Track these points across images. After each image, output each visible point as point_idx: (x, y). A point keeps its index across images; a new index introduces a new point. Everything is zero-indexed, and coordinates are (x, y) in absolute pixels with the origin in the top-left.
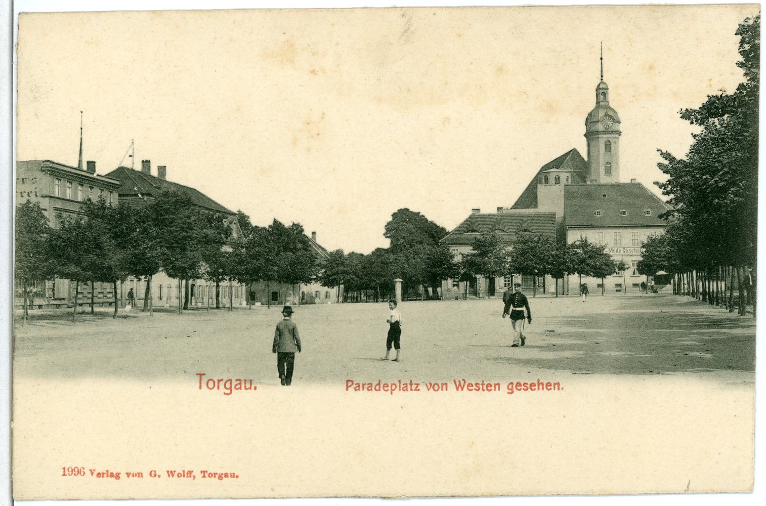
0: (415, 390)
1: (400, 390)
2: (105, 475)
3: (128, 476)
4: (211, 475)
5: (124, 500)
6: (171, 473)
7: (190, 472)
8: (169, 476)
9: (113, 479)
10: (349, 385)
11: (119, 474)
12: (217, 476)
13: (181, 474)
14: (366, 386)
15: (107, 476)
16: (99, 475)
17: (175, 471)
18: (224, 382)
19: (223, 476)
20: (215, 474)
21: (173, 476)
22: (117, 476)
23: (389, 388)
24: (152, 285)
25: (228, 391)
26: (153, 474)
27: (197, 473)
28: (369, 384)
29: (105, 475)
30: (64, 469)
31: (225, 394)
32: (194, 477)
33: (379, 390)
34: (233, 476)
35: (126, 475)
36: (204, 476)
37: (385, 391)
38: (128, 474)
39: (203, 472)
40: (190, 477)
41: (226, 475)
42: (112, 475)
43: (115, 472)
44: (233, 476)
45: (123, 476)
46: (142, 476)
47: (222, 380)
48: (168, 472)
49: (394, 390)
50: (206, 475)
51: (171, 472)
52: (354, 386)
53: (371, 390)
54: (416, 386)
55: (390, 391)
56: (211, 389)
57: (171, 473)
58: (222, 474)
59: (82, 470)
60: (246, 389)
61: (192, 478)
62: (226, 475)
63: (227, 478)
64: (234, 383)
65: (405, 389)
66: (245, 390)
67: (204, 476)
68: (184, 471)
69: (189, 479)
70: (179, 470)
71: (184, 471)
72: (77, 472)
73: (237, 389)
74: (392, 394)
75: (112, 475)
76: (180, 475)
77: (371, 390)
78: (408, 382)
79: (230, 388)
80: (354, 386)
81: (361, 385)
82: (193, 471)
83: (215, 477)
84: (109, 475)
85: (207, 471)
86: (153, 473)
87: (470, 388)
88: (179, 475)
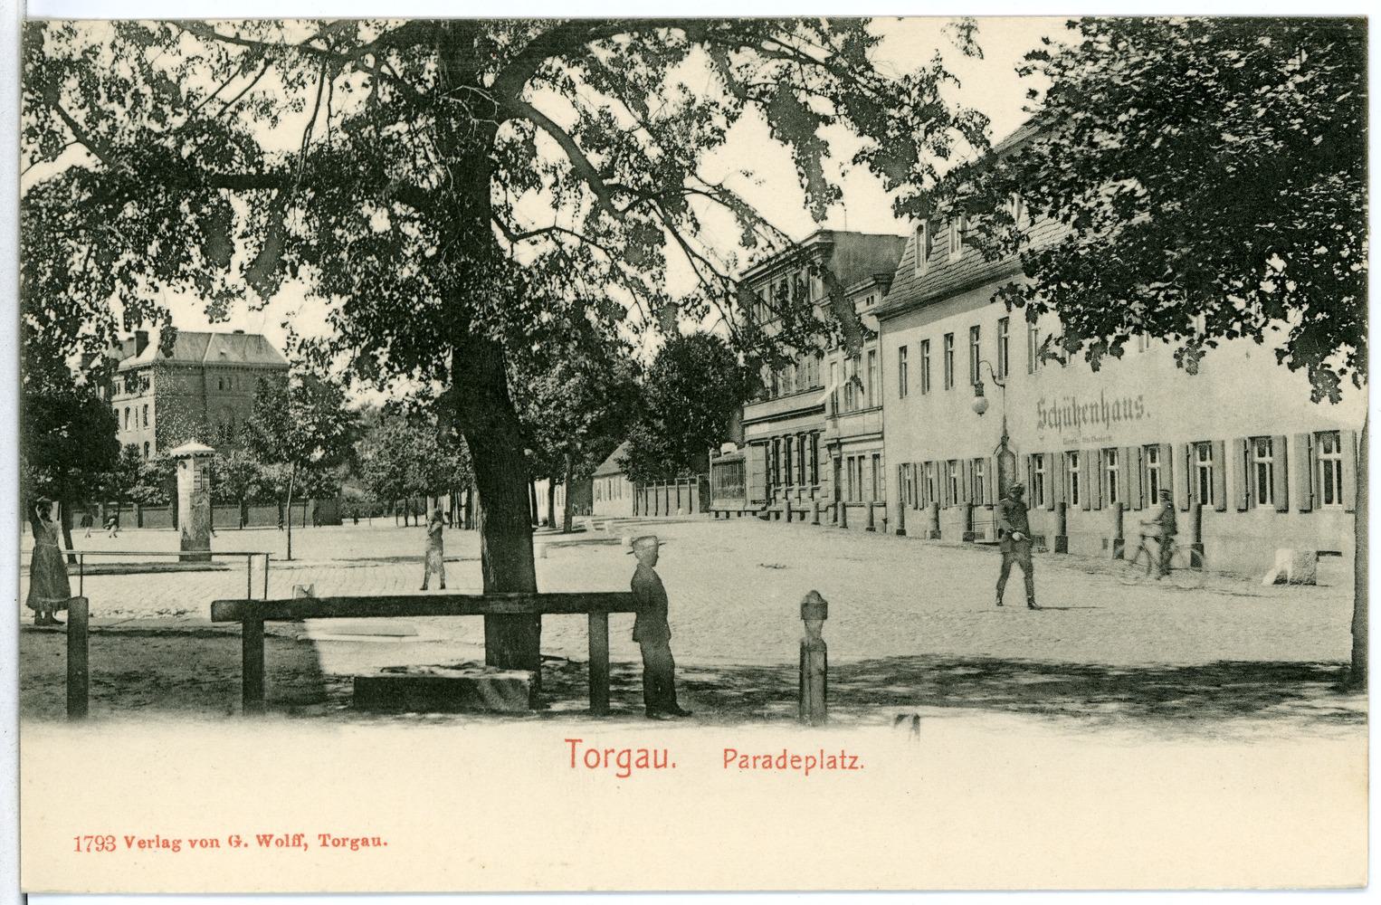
0: (851, 767)
1: (822, 767)
2: (154, 845)
3: (193, 845)
4: (336, 843)
6: (264, 840)
7: (299, 837)
8: (261, 844)
9: (169, 850)
10: (729, 758)
11: (179, 841)
12: (348, 843)
13: (282, 842)
14: (759, 762)
15: (158, 846)
16: (141, 844)
17: (271, 836)
19: (359, 843)
20: (344, 840)
21: (268, 845)
22: (176, 847)
23: (803, 763)
25: (625, 771)
26: (236, 841)
27: (311, 839)
28: (765, 757)
29: (154, 845)
30: (78, 838)
31: (618, 775)
32: (306, 845)
33: (784, 767)
34: (377, 842)
35: (189, 844)
36: (324, 844)
37: (795, 767)
38: (193, 844)
39: (324, 837)
40: (299, 845)
41: (365, 842)
42: (166, 844)
44: (377, 842)
45: (185, 845)
46: (217, 845)
48: (258, 836)
50: (329, 842)
51: (265, 836)
52: (738, 759)
53: (646, 765)
54: (855, 765)
55: (803, 770)
56: (592, 767)
57: (264, 840)
58: (357, 840)
59: (100, 847)
60: (843, 767)
61: (303, 847)
62: (365, 842)
63: (365, 848)
65: (832, 765)
66: (656, 770)
67: (324, 844)
68: (287, 836)
69: (297, 849)
70: (279, 835)
71: (287, 836)
72: (105, 844)
73: (641, 767)
74: (807, 774)
75: (166, 844)
77: (646, 765)
79: (628, 766)
81: (751, 761)
82: (303, 835)
83: (344, 845)
84: (161, 844)
85: (329, 836)
86: (234, 839)
87: (796, 764)
88: (279, 843)
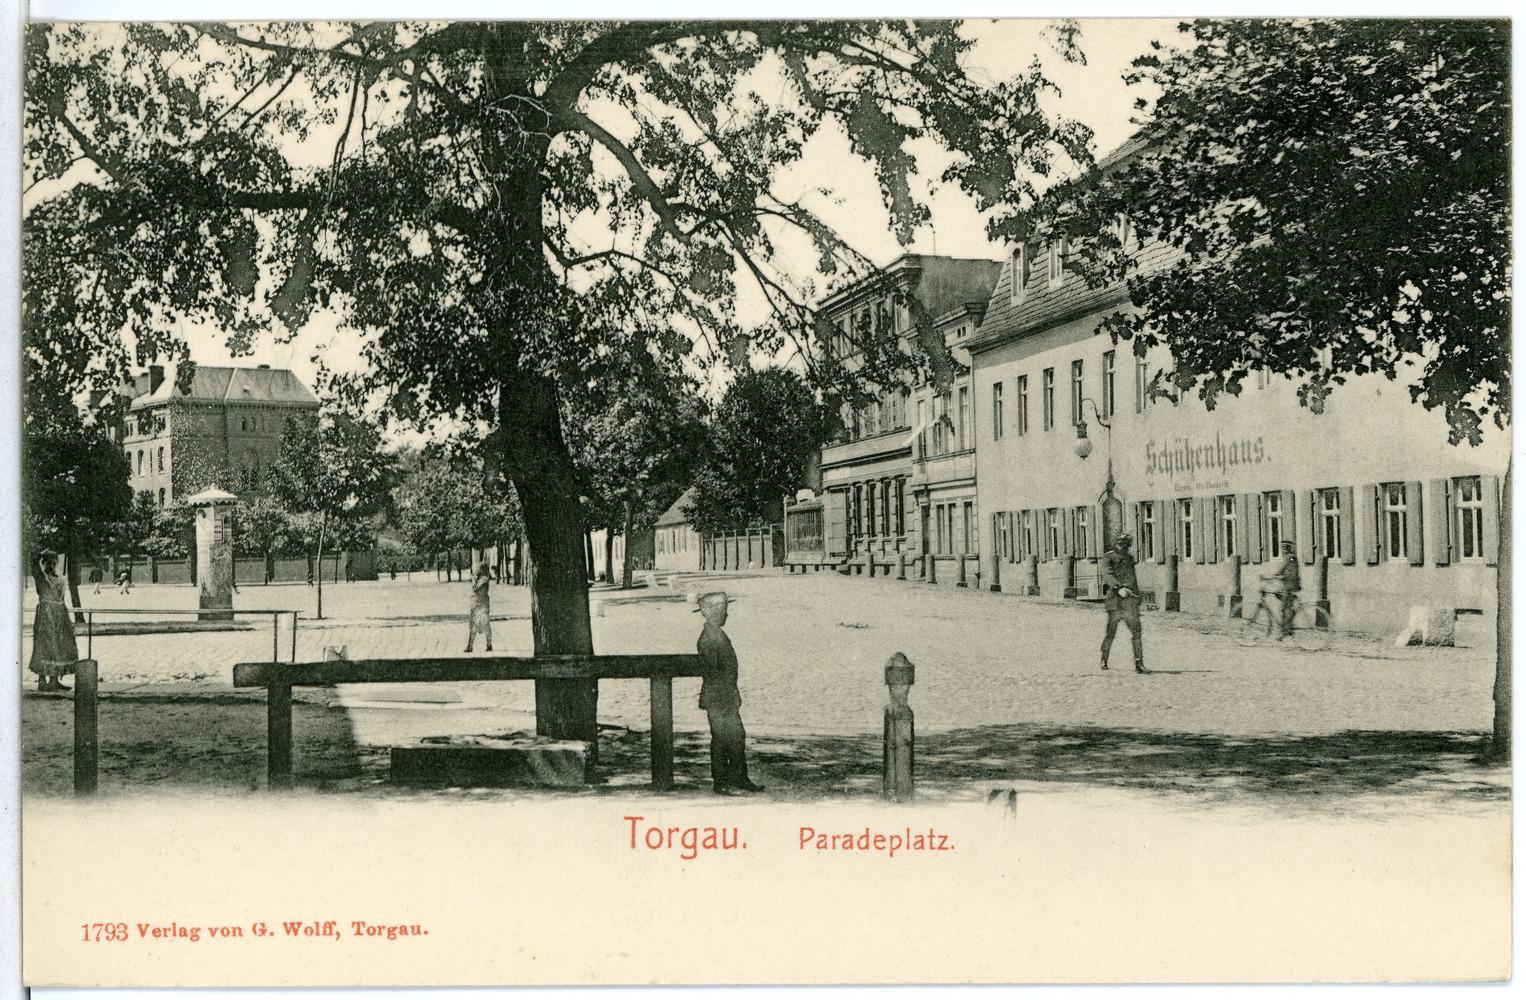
0: (940, 848)
1: (908, 847)
2: (170, 933)
3: (213, 934)
4: (372, 931)
5: (1427, 984)
6: (292, 928)
7: (330, 925)
8: (288, 932)
9: (187, 940)
10: (805, 837)
11: (198, 930)
13: (312, 931)
14: (839, 842)
16: (156, 933)
17: (300, 924)
18: (680, 834)
19: (397, 932)
20: (380, 928)
21: (296, 934)
22: (195, 936)
23: (887, 843)
24: (1152, 727)
25: (690, 852)
26: (261, 930)
27: (344, 927)
28: (845, 836)
29: (170, 933)
30: (86, 926)
31: (683, 857)
32: (338, 934)
33: (867, 847)
34: (417, 930)
36: (359, 933)
37: (878, 848)
38: (213, 932)
39: (358, 925)
40: (331, 933)
41: (403, 930)
42: (183, 933)
43: (401, 938)
44: (417, 930)
45: (204, 934)
46: (240, 934)
47: (677, 830)
48: (285, 924)
49: (862, 837)
50: (363, 930)
51: (292, 924)
52: (816, 839)
55: (887, 851)
56: (654, 848)
57: (292, 928)
58: (395, 928)
62: (403, 930)
64: (702, 835)
65: (919, 845)
66: (724, 851)
67: (359, 933)
68: (317, 924)
70: (308, 922)
71: (317, 924)
72: (116, 932)
73: (709, 847)
74: (891, 855)
75: (183, 933)
76: (371, 931)
78: (926, 834)
79: (694, 846)
80: (816, 839)
81: (829, 841)
82: (335, 923)
83: (380, 933)
84: (178, 932)
85: (364, 923)
86: (258, 927)
88: (309, 931)
